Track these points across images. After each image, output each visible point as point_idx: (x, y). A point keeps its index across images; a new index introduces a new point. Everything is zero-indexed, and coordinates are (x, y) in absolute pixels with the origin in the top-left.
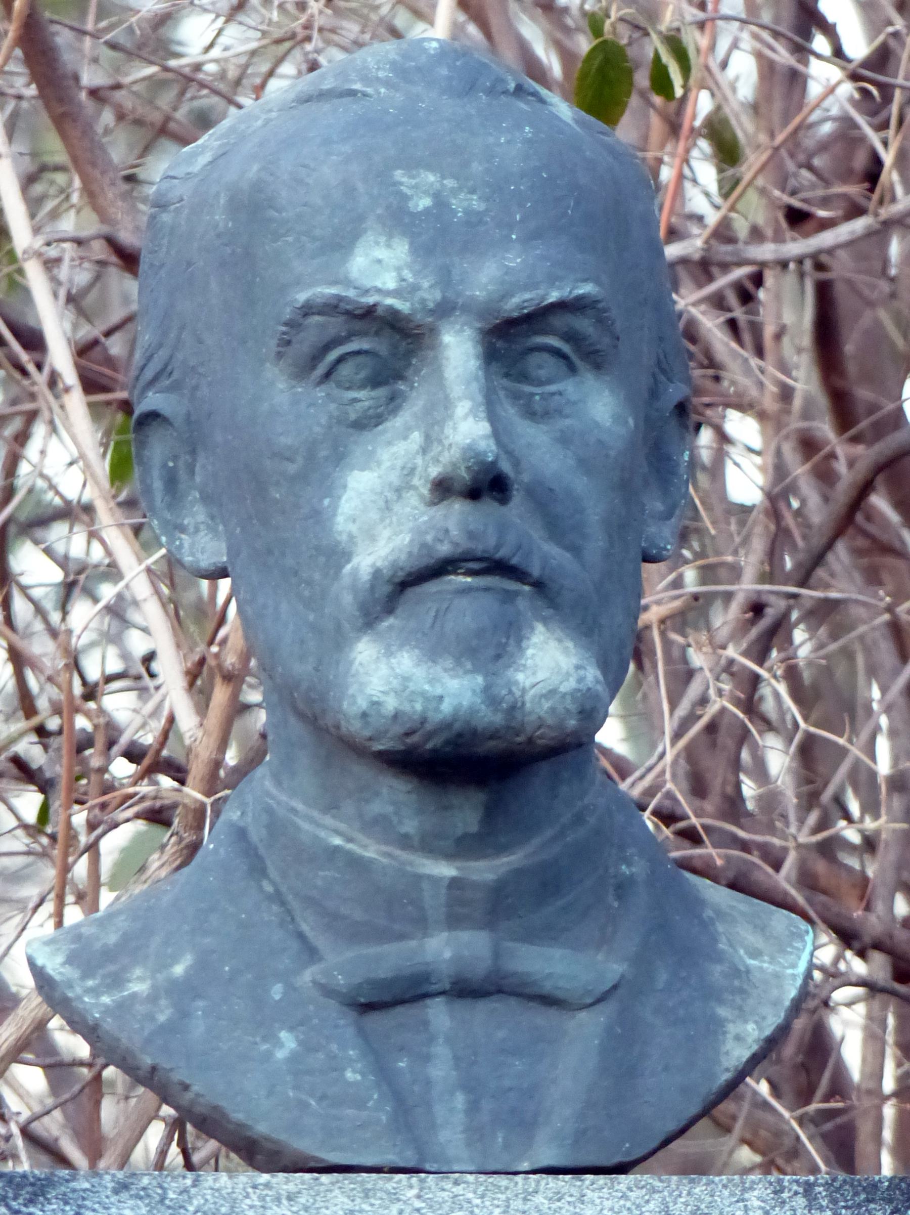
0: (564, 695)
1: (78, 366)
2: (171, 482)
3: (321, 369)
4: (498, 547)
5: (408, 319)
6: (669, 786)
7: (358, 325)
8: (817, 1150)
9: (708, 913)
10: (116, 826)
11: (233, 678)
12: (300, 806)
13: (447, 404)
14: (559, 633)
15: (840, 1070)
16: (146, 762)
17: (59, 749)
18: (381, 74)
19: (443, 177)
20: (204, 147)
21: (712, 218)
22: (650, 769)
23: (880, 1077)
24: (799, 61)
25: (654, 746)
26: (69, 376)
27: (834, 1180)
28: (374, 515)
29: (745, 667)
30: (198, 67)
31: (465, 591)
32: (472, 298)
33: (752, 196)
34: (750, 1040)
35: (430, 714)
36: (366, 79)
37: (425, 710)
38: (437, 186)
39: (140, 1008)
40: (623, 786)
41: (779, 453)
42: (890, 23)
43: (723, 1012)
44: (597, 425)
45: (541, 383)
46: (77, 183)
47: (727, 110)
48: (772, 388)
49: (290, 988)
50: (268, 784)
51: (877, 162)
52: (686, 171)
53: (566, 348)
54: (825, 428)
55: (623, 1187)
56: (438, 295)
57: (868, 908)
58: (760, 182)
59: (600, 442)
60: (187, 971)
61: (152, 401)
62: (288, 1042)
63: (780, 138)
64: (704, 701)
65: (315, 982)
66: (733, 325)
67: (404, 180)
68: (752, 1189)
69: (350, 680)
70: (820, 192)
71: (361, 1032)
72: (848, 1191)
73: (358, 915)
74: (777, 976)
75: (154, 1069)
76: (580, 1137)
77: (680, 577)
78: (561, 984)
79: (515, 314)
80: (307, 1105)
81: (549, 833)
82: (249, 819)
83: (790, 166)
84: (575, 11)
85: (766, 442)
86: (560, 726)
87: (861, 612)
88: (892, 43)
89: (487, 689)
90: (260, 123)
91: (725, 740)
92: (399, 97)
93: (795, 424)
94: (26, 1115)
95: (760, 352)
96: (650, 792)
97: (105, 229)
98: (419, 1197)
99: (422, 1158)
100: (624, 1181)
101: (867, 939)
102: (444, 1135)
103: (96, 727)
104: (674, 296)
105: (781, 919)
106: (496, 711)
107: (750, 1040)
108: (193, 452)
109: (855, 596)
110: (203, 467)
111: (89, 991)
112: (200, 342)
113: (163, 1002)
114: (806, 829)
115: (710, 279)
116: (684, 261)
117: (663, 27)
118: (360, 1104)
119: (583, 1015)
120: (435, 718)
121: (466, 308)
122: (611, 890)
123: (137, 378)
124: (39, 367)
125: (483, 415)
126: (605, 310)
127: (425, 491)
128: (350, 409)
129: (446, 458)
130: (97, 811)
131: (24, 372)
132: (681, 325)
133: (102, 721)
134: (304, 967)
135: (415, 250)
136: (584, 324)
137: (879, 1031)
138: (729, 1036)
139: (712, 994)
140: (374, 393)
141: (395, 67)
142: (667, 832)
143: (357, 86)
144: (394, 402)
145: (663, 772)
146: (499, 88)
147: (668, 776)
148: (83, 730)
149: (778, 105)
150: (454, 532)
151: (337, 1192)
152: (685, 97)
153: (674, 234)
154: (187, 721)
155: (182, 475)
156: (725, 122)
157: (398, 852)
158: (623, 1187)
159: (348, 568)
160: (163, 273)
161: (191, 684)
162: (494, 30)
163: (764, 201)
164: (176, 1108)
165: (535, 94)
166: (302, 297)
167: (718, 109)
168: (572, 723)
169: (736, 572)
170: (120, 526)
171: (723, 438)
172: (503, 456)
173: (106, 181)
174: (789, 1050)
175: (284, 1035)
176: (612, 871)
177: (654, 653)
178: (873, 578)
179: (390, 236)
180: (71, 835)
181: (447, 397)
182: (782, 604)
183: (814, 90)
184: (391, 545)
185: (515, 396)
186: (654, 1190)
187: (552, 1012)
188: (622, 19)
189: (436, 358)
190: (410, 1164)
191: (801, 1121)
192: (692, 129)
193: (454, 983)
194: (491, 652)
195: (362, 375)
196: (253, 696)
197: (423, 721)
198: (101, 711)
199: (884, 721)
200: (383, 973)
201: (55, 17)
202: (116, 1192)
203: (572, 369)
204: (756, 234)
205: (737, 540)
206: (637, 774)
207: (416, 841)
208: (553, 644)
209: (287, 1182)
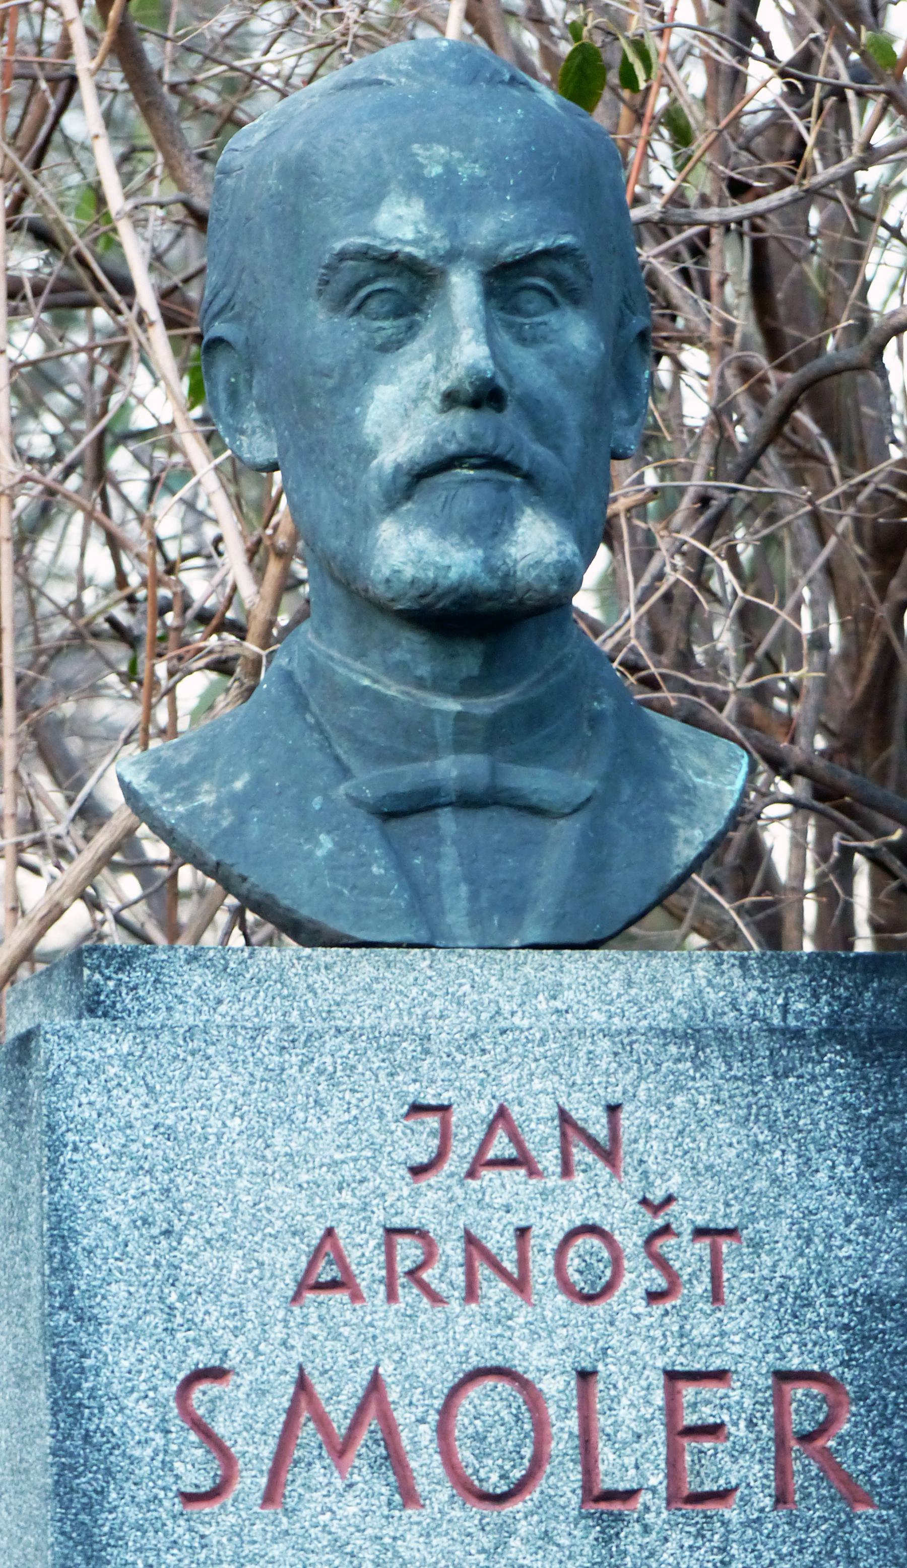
0: (547, 566)
1: (160, 305)
2: (233, 395)
3: (353, 304)
4: (496, 446)
5: (423, 263)
6: (634, 642)
7: (384, 269)
8: (753, 936)
9: (664, 741)
10: (190, 672)
11: (283, 555)
12: (336, 654)
13: (455, 332)
14: (544, 515)
15: (770, 874)
16: (214, 622)
17: (144, 612)
18: (402, 67)
19: (451, 150)
20: (260, 126)
21: (669, 187)
22: (618, 629)
23: (802, 879)
24: (739, 62)
25: (621, 612)
26: (153, 313)
27: (764, 955)
28: (396, 421)
29: (694, 547)
30: (258, 67)
31: (468, 481)
32: (475, 247)
33: (701, 170)
34: (697, 842)
35: (440, 580)
36: (390, 71)
37: (436, 578)
38: (447, 157)
39: (208, 816)
40: (598, 642)
41: (722, 377)
42: (813, 31)
43: (675, 820)
44: (574, 348)
45: (529, 315)
46: (160, 158)
47: (681, 101)
48: (717, 324)
49: (327, 798)
50: (310, 636)
51: (802, 144)
52: (650, 153)
53: (549, 287)
54: (760, 359)
55: (594, 960)
56: (447, 244)
57: (793, 741)
58: (707, 158)
59: (577, 363)
60: (245, 787)
61: (219, 329)
62: (326, 842)
63: (724, 122)
64: (660, 576)
65: (348, 796)
66: (685, 274)
67: (421, 152)
68: (697, 961)
69: (376, 552)
70: (756, 168)
71: (387, 838)
72: (775, 963)
73: (382, 741)
74: (719, 792)
75: (218, 864)
76: (560, 920)
77: (642, 475)
78: (545, 797)
79: (510, 260)
80: (341, 894)
81: (535, 676)
82: (295, 664)
83: (733, 147)
84: (560, 23)
85: (713, 369)
86: (545, 589)
87: (789, 504)
88: (814, 48)
89: (486, 561)
90: (305, 106)
91: (680, 607)
92: (416, 86)
93: (734, 353)
94: (116, 905)
95: (707, 296)
96: (618, 647)
97: (183, 195)
98: (430, 967)
99: (433, 935)
100: (595, 954)
101: (792, 766)
102: (451, 918)
103: (175, 594)
104: (638, 250)
105: (722, 746)
106: (492, 578)
107: (697, 842)
108: (251, 370)
109: (783, 490)
110: (259, 382)
111: (166, 802)
112: (256, 281)
113: (226, 811)
114: (743, 679)
115: (668, 237)
116: (646, 221)
117: (629, 34)
118: (383, 892)
119: (562, 822)
120: (444, 583)
121: (471, 255)
122: (585, 724)
123: (206, 311)
124: (130, 307)
125: (483, 340)
126: (582, 257)
127: (437, 401)
128: (376, 335)
129: (454, 375)
130: (175, 662)
131: (119, 312)
132: (644, 274)
133: (179, 589)
134: (339, 783)
135: (428, 208)
136: (565, 269)
137: (801, 840)
138: (680, 840)
139: (667, 806)
140: (395, 323)
141: (413, 62)
142: (632, 679)
143: (383, 77)
144: (412, 331)
145: (628, 632)
146: (497, 79)
147: (632, 634)
148: (165, 598)
149: (722, 99)
150: (460, 435)
151: (365, 963)
152: (648, 89)
153: (638, 201)
154: (247, 589)
155: (243, 389)
156: (679, 111)
157: (414, 691)
158: (594, 960)
159: (375, 463)
160: (227, 227)
161: (251, 560)
162: (495, 38)
163: (710, 175)
164: (237, 896)
165: (526, 84)
166: (338, 246)
167: (675, 100)
168: (554, 587)
169: (687, 472)
170: (194, 432)
171: (679, 367)
172: (499, 374)
173: (183, 157)
174: (730, 858)
175: (323, 837)
176: (586, 707)
177: (621, 536)
178: (798, 479)
179: (409, 197)
180: (155, 682)
181: (454, 328)
182: (725, 497)
183: (752, 85)
184: (409, 445)
185: (509, 326)
186: (619, 963)
187: (537, 820)
188: (596, 27)
189: (445, 295)
190: (424, 941)
191: (739, 911)
192: (653, 118)
193: (460, 797)
194: (489, 530)
195: (387, 307)
196: (302, 572)
197: (435, 586)
198: (179, 582)
199: (806, 593)
200: (402, 787)
201: (142, 26)
202: (188, 962)
203: (555, 304)
204: (705, 201)
205: (689, 445)
206: (608, 633)
207: (429, 683)
208: (539, 524)
209: (325, 954)
